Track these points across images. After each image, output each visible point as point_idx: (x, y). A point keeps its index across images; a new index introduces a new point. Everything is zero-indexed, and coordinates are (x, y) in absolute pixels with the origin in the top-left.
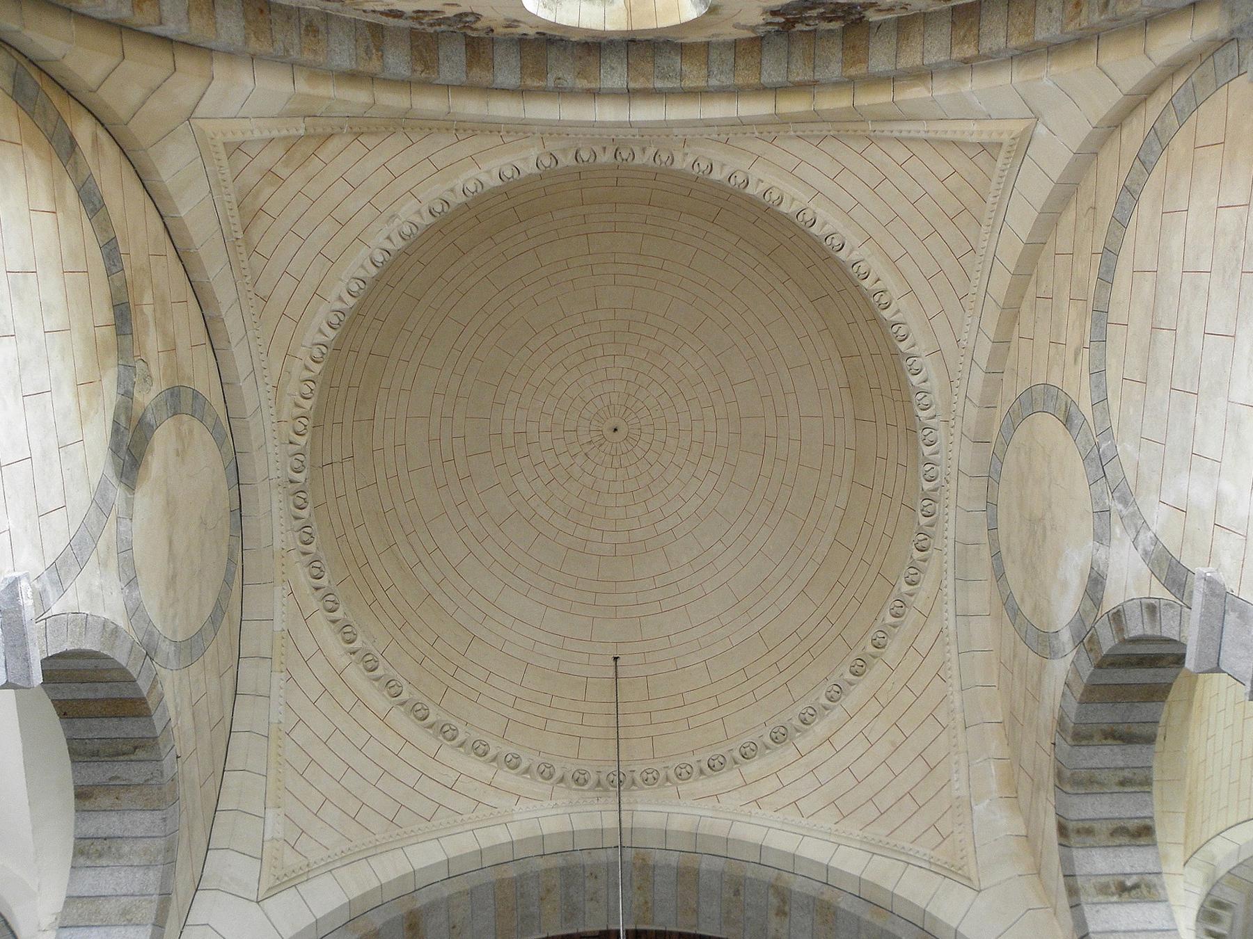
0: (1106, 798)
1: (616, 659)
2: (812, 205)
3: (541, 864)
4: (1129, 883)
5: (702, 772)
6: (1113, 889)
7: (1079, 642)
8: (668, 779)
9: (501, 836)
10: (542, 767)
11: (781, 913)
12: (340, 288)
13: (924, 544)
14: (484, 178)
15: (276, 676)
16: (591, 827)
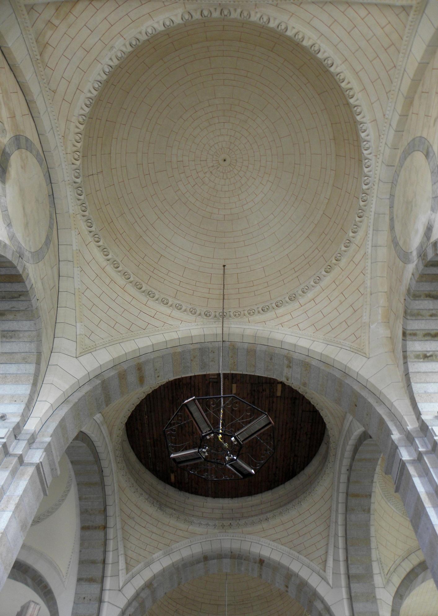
0: (423, 321)
1: (224, 266)
2: (319, 42)
3: (192, 347)
4: (428, 355)
5: (259, 312)
6: (421, 356)
7: (419, 256)
8: (244, 315)
9: (174, 336)
10: (191, 310)
11: (289, 367)
12: (89, 86)
13: (361, 214)
14: (156, 26)
15: (76, 269)
16: (211, 333)
